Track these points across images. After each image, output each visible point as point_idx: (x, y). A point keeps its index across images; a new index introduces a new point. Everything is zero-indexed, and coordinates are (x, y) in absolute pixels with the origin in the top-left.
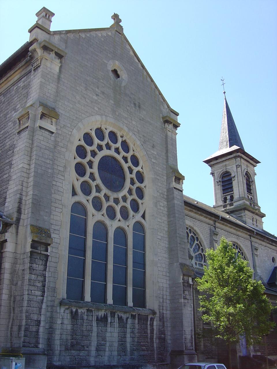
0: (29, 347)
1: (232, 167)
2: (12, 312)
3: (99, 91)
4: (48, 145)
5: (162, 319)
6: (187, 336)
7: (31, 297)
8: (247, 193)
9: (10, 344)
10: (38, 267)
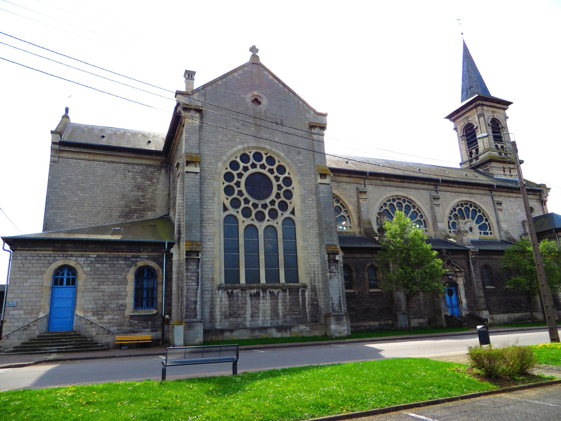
0: (190, 318)
1: (473, 118)
2: (180, 297)
3: (239, 125)
4: (194, 183)
5: (314, 289)
6: (335, 301)
7: (188, 287)
8: (493, 142)
9: (180, 317)
10: (193, 267)
